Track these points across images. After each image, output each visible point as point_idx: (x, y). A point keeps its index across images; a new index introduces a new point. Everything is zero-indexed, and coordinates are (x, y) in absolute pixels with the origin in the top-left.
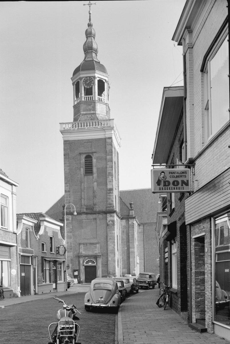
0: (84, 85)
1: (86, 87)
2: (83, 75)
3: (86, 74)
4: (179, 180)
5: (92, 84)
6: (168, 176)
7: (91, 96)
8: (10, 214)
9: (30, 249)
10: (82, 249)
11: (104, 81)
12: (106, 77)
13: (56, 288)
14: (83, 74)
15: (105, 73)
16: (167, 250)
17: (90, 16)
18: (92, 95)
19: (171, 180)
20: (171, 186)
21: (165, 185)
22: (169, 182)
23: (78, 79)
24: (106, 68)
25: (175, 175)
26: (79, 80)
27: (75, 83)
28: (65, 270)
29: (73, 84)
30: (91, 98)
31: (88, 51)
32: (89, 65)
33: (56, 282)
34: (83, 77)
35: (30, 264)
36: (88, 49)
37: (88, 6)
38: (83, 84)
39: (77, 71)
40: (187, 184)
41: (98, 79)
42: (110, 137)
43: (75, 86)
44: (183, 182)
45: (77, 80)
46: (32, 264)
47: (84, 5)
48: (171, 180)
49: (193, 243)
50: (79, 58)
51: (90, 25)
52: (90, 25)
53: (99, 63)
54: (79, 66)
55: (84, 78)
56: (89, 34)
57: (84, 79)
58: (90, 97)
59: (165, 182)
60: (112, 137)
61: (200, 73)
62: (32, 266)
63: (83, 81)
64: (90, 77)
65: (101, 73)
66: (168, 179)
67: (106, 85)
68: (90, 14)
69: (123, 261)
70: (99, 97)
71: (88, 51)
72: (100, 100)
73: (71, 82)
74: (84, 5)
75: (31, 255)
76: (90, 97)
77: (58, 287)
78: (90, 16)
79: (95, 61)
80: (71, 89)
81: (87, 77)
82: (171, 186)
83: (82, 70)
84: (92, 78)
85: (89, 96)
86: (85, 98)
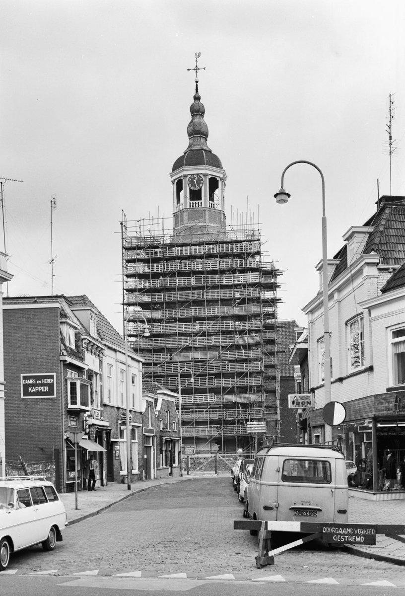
0: (190, 185)
1: (192, 188)
2: (189, 171)
3: (192, 170)
4: (306, 401)
5: (201, 185)
6: (299, 398)
7: (200, 201)
8: (360, 493)
9: (152, 428)
11: (218, 179)
12: (221, 173)
13: (171, 474)
14: (187, 170)
15: (219, 167)
16: (301, 436)
17: (197, 85)
18: (201, 199)
19: (301, 401)
20: (301, 404)
21: (297, 404)
22: (299, 402)
23: (181, 177)
24: (221, 161)
25: (303, 398)
26: (182, 178)
27: (176, 181)
28: (179, 450)
29: (173, 182)
31: (195, 136)
32: (197, 154)
33: (171, 466)
34: (189, 175)
35: (151, 445)
36: (197, 132)
37: (194, 72)
39: (178, 165)
40: (310, 404)
41: (210, 177)
43: (175, 185)
44: (308, 402)
45: (179, 177)
46: (153, 445)
47: (188, 70)
48: (301, 401)
49: (315, 438)
50: (181, 145)
51: (197, 98)
52: (197, 98)
53: (211, 152)
54: (182, 157)
55: (189, 176)
56: (197, 111)
57: (190, 177)
59: (297, 403)
61: (316, 342)
62: (152, 448)
63: (188, 180)
64: (198, 174)
65: (214, 168)
66: (299, 401)
67: (220, 183)
68: (197, 82)
70: (211, 202)
71: (195, 136)
72: (212, 207)
73: (170, 180)
74: (188, 70)
75: (152, 435)
77: (173, 472)
78: (197, 85)
79: (204, 150)
80: (172, 189)
81: (193, 175)
82: (301, 404)
83: (186, 165)
84: (201, 175)
85: (197, 202)
86: (190, 204)
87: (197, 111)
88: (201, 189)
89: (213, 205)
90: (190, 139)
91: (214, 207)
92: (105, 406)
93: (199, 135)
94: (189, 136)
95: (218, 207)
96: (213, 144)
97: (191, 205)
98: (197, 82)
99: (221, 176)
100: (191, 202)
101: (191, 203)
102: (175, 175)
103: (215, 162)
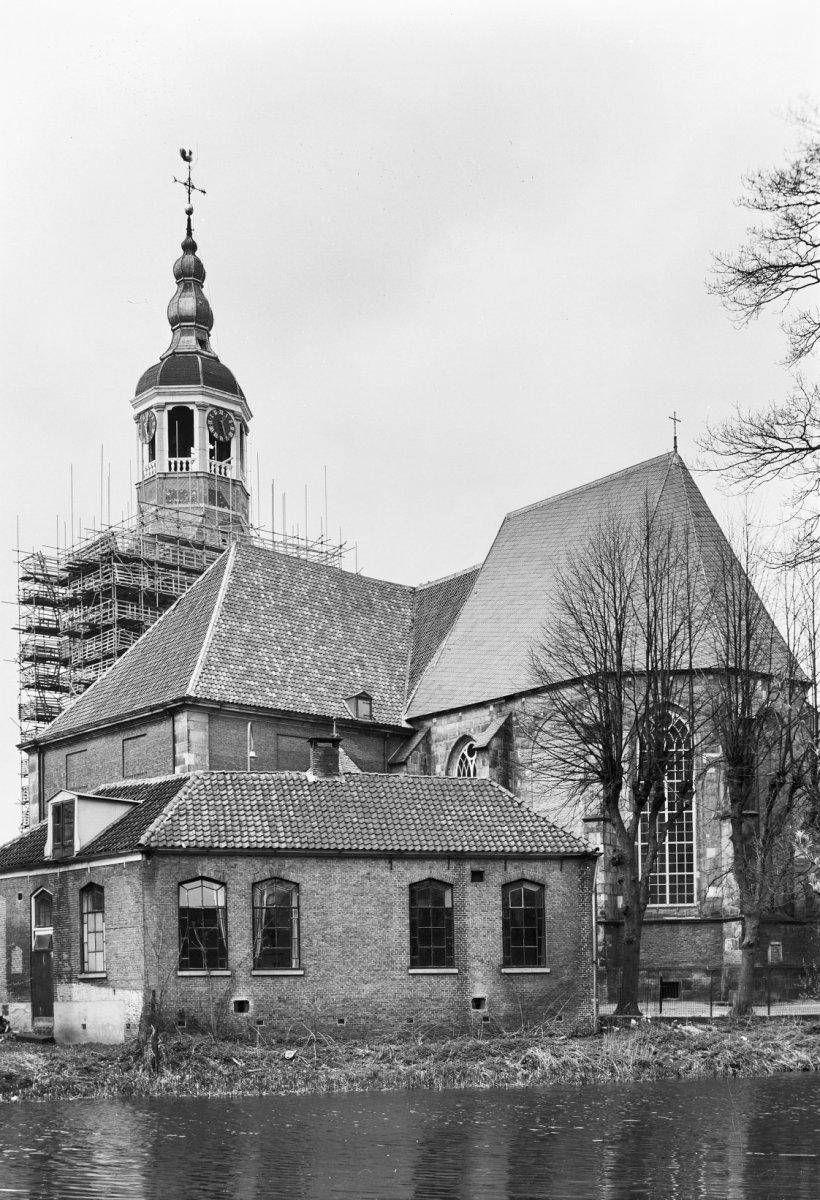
0: (212, 429)
5: (230, 434)
10: (85, 615)
11: (191, 407)
12: (236, 403)
17: (189, 220)
30: (184, 465)
31: (183, 324)
38: (208, 425)
42: (425, 964)
50: (158, 342)
51: (190, 247)
52: (190, 247)
55: (210, 409)
56: (191, 275)
57: (211, 412)
58: (181, 463)
60: (414, 964)
68: (189, 212)
69: (58, 735)
74: (204, 192)
76: (181, 463)
78: (189, 220)
86: (170, 463)
87: (191, 275)
88: (230, 442)
89: (223, 470)
90: (173, 331)
91: (225, 474)
92: (223, 884)
93: (193, 324)
94: (172, 324)
95: (232, 474)
96: (222, 344)
97: (173, 466)
98: (189, 212)
99: (238, 409)
100: (173, 460)
101: (179, 462)
102: (142, 402)
103: (223, 380)
